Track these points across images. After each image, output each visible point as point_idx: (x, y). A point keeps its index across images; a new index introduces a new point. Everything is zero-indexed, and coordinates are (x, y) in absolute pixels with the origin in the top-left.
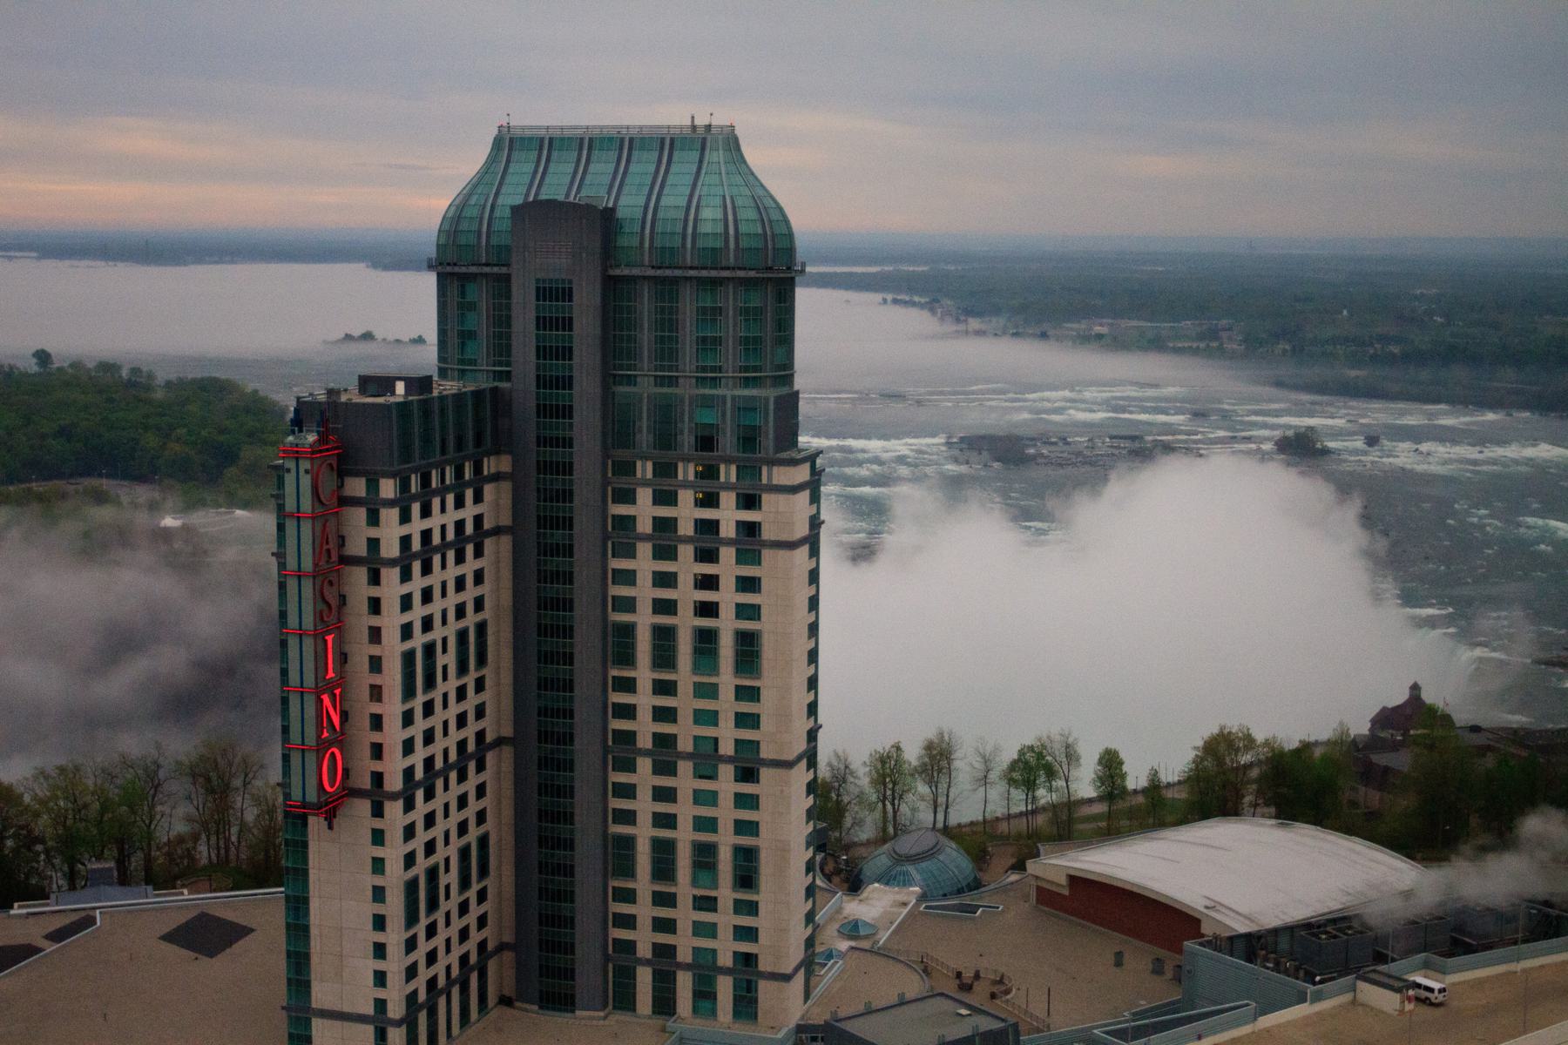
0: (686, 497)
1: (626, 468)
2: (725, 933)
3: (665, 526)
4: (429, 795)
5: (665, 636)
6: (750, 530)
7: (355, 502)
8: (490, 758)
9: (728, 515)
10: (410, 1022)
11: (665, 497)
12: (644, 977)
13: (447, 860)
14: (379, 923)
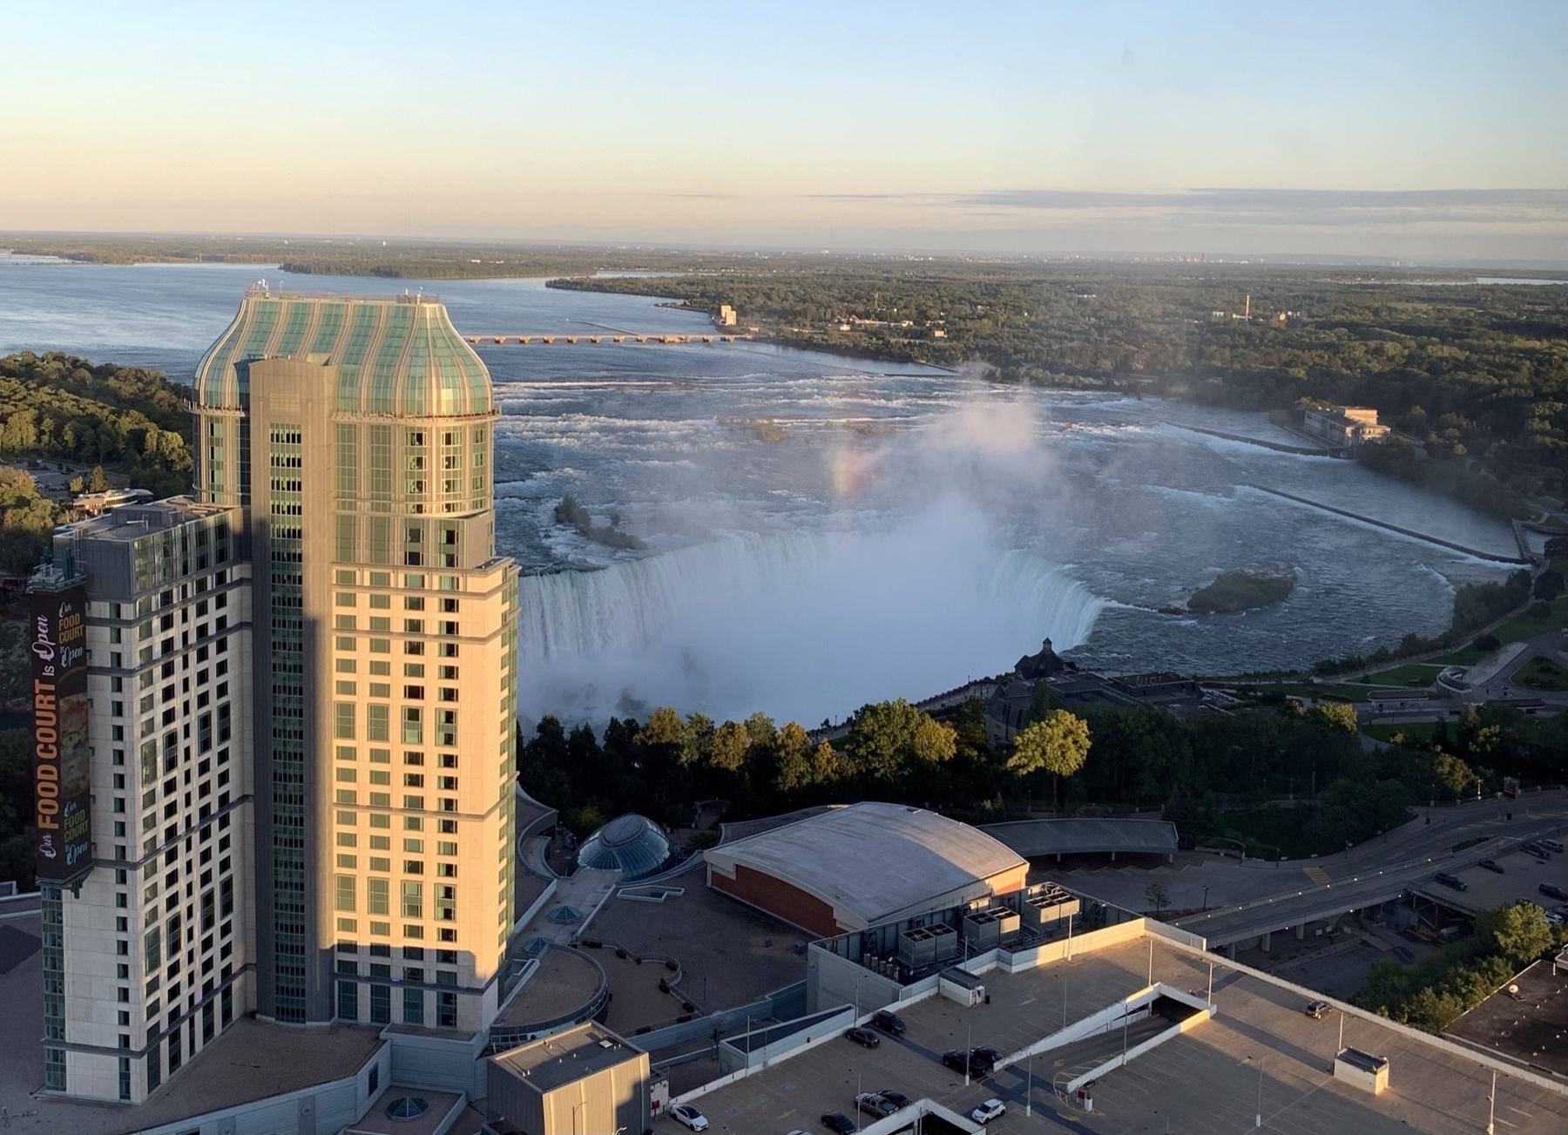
3: (380, 625)
7: (101, 622)
10: (152, 1054)
11: (380, 602)
12: (364, 992)
13: (187, 727)
14: (124, 971)
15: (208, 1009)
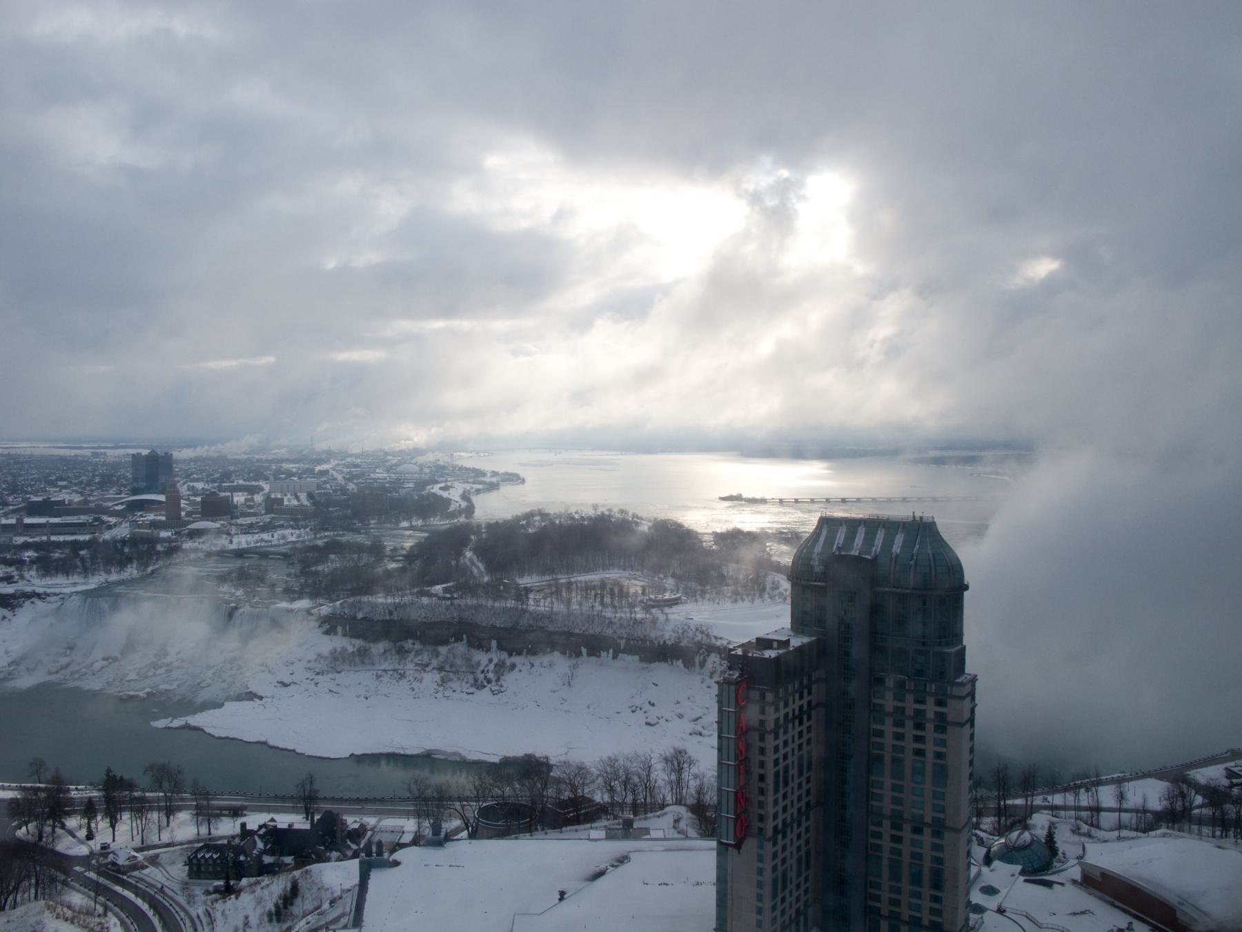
4: (786, 732)
5: (897, 762)
6: (941, 717)
8: (814, 713)
9: (931, 709)
15: (797, 924)
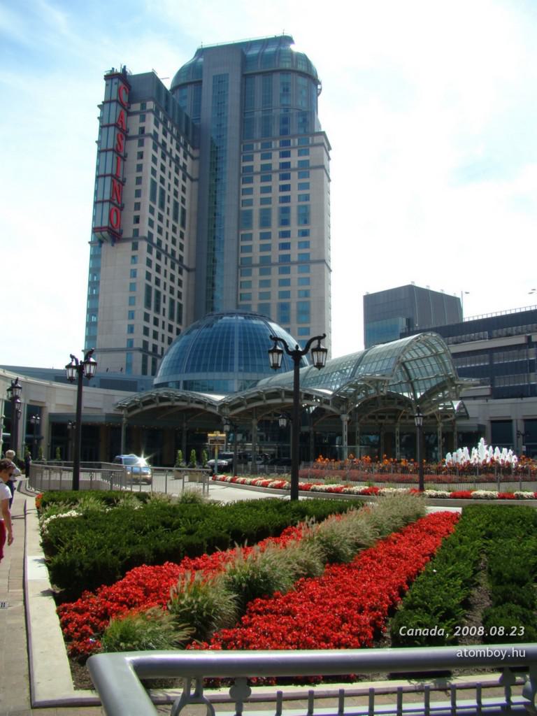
0: (276, 154)
1: (250, 147)
2: (294, 281)
3: (266, 168)
